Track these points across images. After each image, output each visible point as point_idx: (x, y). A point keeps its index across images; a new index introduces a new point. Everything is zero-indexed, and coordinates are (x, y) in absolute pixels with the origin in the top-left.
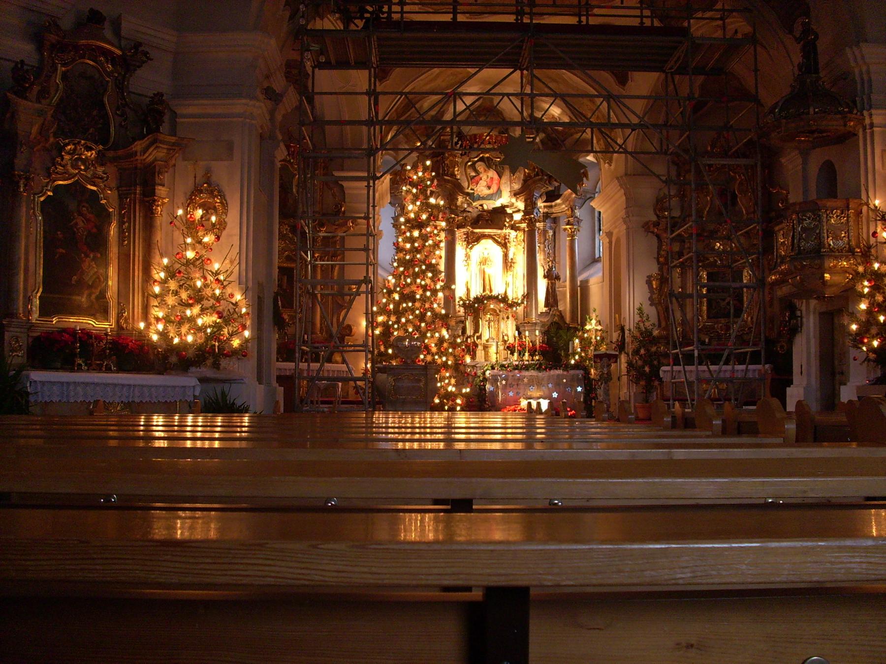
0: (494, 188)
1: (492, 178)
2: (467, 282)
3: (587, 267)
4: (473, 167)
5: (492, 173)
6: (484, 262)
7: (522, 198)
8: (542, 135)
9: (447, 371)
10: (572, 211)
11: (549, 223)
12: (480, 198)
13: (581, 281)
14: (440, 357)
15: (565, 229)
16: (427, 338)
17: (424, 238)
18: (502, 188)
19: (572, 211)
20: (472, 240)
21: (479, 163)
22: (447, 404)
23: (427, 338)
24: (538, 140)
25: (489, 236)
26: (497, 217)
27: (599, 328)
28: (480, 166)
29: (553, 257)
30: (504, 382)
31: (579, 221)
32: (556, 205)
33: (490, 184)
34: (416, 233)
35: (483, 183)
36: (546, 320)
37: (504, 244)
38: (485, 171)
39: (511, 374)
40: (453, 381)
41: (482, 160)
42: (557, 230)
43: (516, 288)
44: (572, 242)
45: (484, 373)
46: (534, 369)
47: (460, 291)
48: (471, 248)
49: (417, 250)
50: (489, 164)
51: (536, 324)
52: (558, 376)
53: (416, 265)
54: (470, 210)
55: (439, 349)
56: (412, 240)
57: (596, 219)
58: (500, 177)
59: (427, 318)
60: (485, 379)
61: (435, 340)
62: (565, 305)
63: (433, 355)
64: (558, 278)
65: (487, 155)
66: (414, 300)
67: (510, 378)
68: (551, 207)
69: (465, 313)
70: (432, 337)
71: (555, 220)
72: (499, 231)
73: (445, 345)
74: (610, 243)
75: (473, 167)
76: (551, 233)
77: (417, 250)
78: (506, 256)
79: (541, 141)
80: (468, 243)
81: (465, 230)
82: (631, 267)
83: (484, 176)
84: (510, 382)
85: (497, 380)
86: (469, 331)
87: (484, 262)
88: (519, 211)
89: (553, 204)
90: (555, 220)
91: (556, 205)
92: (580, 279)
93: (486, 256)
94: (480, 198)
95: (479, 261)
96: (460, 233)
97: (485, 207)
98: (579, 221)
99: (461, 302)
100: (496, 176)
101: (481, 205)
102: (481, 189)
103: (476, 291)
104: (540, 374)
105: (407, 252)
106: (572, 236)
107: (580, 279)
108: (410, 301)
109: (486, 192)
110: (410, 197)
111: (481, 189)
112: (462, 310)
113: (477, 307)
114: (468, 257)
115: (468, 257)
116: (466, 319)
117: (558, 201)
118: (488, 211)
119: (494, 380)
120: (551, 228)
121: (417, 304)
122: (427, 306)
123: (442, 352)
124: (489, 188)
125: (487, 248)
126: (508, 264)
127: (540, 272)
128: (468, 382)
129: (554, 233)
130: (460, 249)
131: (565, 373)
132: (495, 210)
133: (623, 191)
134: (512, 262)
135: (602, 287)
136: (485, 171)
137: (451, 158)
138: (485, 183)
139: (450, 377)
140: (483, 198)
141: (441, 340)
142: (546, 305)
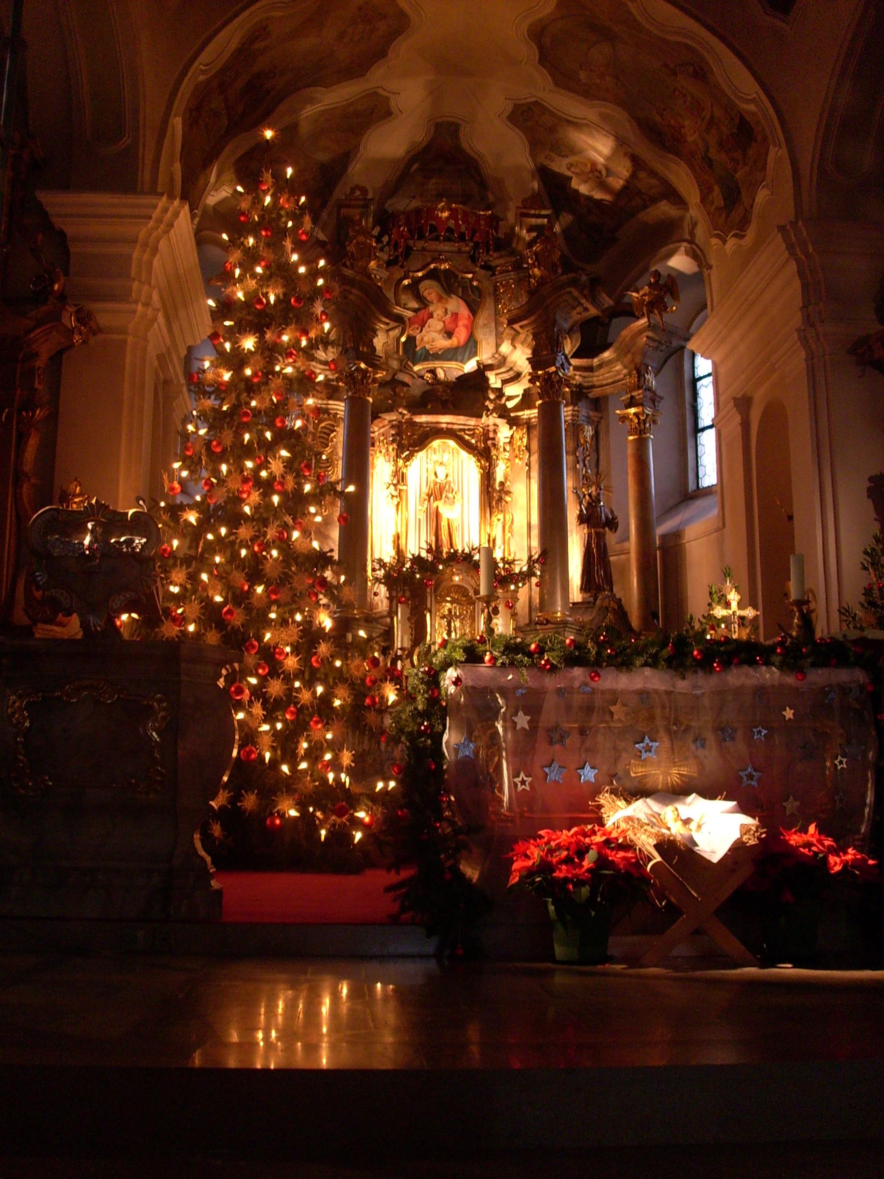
0: (461, 335)
1: (455, 316)
2: (393, 527)
3: (669, 510)
4: (414, 289)
5: (455, 304)
6: (437, 492)
7: (526, 335)
8: (567, 218)
9: (327, 726)
10: (640, 375)
11: (584, 410)
12: (427, 356)
13: (663, 537)
14: (309, 684)
15: (624, 418)
16: (267, 623)
17: (270, 351)
18: (480, 335)
19: (640, 375)
20: (410, 441)
21: (427, 283)
22: (323, 823)
23: (267, 623)
24: (557, 228)
25: (450, 433)
26: (470, 393)
27: (749, 613)
28: (430, 290)
29: (595, 475)
30: (522, 721)
31: (654, 400)
32: (600, 366)
33: (450, 327)
34: (249, 343)
35: (435, 325)
36: (412, 872)
37: (484, 451)
38: (440, 299)
39: (551, 682)
40: (346, 758)
41: (433, 275)
42: (602, 427)
43: (516, 536)
44: (641, 445)
45: (433, 679)
46: (653, 663)
47: (381, 547)
48: (408, 459)
49: (251, 388)
50: (449, 284)
51: (564, 624)
52: (761, 691)
53: (247, 427)
54: (406, 379)
55: (305, 661)
56: (237, 361)
57: (688, 406)
58: (474, 310)
59: (268, 567)
60: (437, 709)
61: (292, 634)
62: (630, 588)
63: (288, 679)
64: (612, 524)
65: (445, 266)
66: (235, 520)
67: (550, 702)
68: (590, 369)
69: (390, 599)
70: (283, 622)
71: (599, 404)
72: (472, 422)
73: (323, 649)
74: (745, 425)
75: (414, 289)
76: (589, 431)
77: (251, 388)
78: (487, 477)
79: (565, 232)
80: (401, 448)
81: (393, 417)
82: (826, 455)
83: (438, 312)
84: (548, 717)
85: (489, 713)
86: (401, 639)
87: (437, 492)
88: (517, 377)
89: (596, 361)
90: (599, 404)
91: (600, 366)
92: (660, 530)
93: (441, 478)
94: (427, 356)
95: (425, 490)
96: (378, 430)
97: (441, 374)
98: (654, 400)
99: (381, 573)
100: (464, 311)
101: (433, 372)
102: (432, 337)
103: (416, 545)
104: (682, 685)
105: (220, 390)
106: (641, 431)
107: (660, 530)
108: (222, 521)
109: (443, 343)
110: (236, 256)
111: (432, 337)
112: (383, 590)
113: (419, 580)
114: (400, 478)
115: (400, 478)
116: (392, 613)
117: (607, 355)
118: (447, 384)
119: (480, 707)
120: (590, 421)
121: (244, 532)
122: (271, 533)
123: (313, 671)
124: (449, 334)
125: (446, 463)
126: (492, 496)
127: (572, 513)
128: (176, 454)
129: (596, 436)
130: (381, 467)
131: (790, 680)
132: (464, 379)
133: (793, 266)
134: (504, 491)
135: (720, 543)
136: (440, 299)
137: (361, 238)
138: (440, 326)
139: (336, 747)
140: (436, 357)
141: (310, 636)
142: (584, 588)
